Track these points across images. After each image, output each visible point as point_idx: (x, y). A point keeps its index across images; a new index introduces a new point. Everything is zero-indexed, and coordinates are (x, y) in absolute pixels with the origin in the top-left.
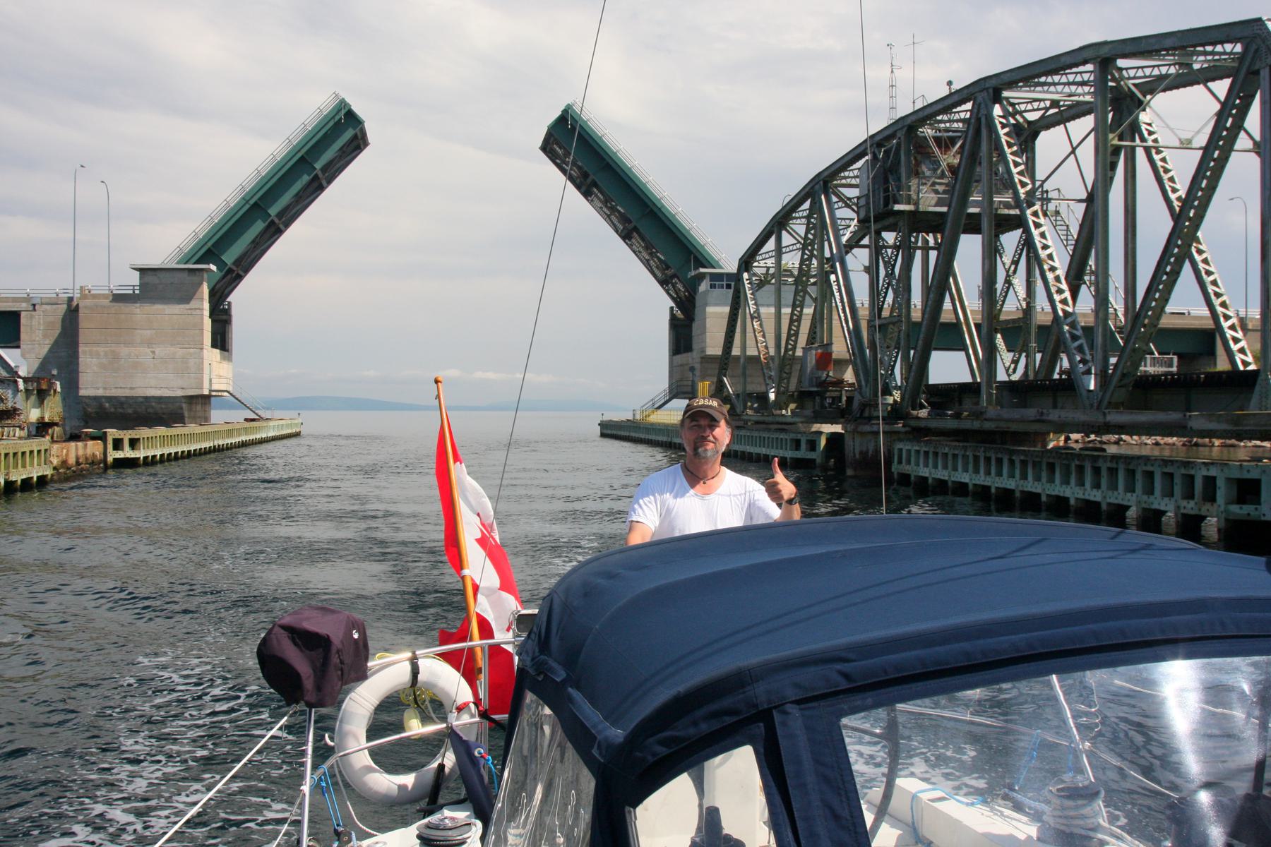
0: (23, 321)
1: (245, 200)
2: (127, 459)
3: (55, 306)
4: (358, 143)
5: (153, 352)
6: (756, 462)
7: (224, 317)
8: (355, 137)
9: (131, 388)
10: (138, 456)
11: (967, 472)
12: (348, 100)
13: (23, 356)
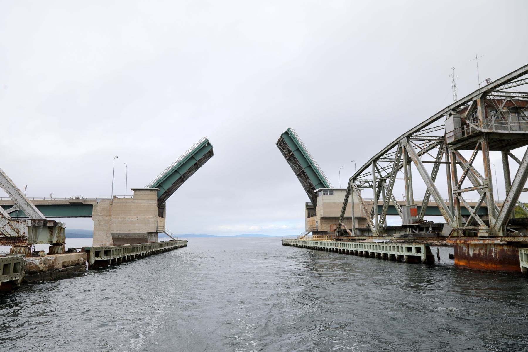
0: (93, 208)
1: (173, 169)
2: (103, 260)
3: (105, 203)
4: (210, 154)
5: (137, 218)
6: (371, 257)
7: (163, 207)
8: (209, 152)
9: (130, 230)
10: (109, 259)
11: (399, 251)
12: (208, 139)
13: (93, 219)
